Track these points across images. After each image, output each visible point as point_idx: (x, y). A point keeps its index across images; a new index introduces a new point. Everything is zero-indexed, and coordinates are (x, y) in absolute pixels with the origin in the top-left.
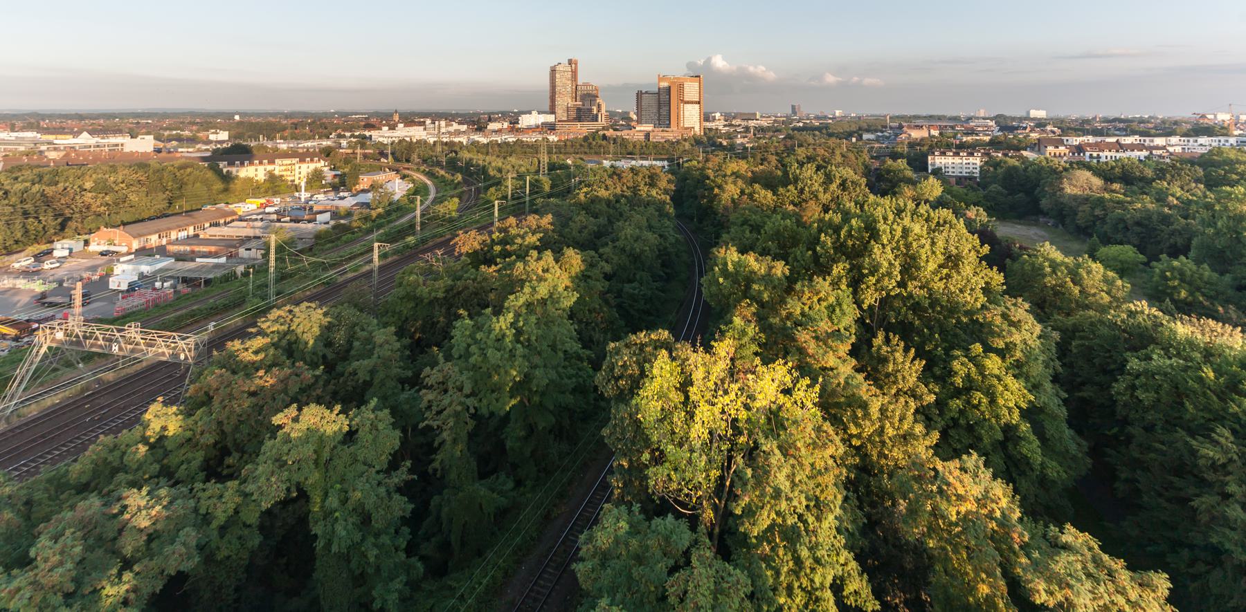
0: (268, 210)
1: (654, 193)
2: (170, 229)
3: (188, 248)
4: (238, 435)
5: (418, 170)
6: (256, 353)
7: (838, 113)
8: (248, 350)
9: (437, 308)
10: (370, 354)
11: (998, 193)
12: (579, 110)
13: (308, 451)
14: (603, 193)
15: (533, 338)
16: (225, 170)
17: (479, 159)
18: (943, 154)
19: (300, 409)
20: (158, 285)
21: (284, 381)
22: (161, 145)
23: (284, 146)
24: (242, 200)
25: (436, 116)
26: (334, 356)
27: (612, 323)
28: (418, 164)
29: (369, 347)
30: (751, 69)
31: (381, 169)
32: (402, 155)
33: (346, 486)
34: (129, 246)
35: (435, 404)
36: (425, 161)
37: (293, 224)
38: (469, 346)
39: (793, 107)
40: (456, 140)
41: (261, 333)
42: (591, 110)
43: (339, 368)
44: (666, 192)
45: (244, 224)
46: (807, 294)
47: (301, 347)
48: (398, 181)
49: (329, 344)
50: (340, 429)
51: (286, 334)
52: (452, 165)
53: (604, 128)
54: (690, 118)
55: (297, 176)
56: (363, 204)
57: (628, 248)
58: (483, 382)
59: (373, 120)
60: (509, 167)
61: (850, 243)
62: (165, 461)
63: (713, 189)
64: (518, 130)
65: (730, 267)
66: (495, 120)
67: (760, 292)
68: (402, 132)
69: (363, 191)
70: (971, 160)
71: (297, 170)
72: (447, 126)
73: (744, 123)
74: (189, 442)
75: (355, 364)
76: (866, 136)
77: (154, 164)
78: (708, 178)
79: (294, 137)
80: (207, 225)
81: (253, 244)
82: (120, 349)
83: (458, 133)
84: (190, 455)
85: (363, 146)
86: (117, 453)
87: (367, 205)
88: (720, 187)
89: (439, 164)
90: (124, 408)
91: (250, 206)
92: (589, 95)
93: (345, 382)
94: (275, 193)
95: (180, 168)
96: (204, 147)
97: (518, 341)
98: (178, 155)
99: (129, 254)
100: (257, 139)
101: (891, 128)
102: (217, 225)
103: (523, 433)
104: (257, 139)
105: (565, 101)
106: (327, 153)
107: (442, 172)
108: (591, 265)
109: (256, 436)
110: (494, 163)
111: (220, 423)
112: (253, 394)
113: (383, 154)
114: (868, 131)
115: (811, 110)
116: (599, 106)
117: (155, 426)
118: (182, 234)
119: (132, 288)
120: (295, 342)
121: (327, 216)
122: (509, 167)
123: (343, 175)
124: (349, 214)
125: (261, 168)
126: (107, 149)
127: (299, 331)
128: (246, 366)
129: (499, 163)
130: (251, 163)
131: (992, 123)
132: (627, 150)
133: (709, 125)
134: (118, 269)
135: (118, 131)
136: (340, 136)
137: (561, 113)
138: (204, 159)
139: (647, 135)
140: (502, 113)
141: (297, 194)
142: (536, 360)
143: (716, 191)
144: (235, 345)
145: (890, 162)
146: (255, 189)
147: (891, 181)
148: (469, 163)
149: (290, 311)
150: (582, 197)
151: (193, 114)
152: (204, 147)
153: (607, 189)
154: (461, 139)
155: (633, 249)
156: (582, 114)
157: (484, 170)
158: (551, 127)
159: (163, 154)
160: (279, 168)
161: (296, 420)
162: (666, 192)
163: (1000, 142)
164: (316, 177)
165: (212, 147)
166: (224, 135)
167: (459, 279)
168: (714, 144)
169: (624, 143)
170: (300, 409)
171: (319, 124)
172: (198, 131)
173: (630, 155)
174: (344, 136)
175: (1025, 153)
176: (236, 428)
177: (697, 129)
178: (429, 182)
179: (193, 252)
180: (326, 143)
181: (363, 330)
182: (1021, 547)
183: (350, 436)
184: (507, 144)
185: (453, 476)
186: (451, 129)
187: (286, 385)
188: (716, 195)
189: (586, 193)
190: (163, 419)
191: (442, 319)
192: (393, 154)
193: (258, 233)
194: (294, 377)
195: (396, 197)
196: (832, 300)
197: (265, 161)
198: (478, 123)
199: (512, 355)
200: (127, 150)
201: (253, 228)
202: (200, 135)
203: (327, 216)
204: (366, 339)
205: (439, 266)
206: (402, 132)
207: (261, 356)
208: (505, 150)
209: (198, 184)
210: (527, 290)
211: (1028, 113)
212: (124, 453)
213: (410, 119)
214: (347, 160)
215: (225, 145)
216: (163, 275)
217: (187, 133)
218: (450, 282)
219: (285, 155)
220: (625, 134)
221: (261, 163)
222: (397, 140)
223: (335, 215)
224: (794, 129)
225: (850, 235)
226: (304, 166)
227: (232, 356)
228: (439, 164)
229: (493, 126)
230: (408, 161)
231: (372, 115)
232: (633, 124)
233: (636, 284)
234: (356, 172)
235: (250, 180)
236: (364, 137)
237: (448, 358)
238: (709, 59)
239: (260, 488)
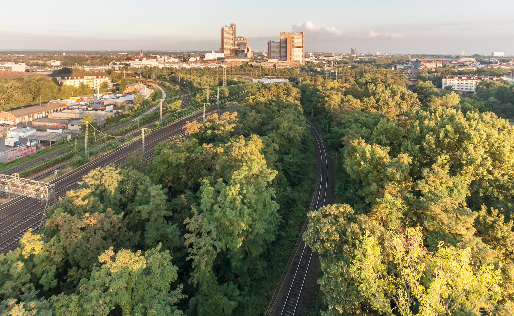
0: (81, 103)
1: (290, 99)
2: (34, 113)
3: (43, 124)
4: (75, 255)
5: (155, 83)
6: (83, 199)
7: (378, 53)
8: (79, 197)
9: (181, 169)
10: (148, 202)
11: (493, 102)
12: (237, 51)
13: (122, 283)
14: (263, 100)
15: (253, 201)
16: (60, 82)
17: (188, 77)
18: (452, 78)
19: (115, 252)
20: (28, 144)
21: (101, 222)
22: (29, 68)
23: (87, 69)
24: (68, 98)
25: (162, 54)
26: (126, 199)
27: (280, 180)
28: (155, 79)
29: (147, 195)
30: (328, 29)
31: (136, 82)
32: (146, 74)
33: (145, 305)
34: (15, 122)
35: (195, 244)
36: (158, 78)
37: (94, 112)
38: (213, 205)
39: (352, 50)
40: (174, 66)
41: (86, 186)
42: (243, 51)
43: (129, 207)
44: (296, 99)
45: (70, 111)
46: (432, 178)
47: (108, 194)
48: (146, 88)
49: (122, 192)
50: (142, 266)
51: (99, 186)
52: (173, 80)
53: (250, 61)
54: (297, 56)
55: (95, 85)
56: (129, 101)
57: (285, 134)
58: (225, 231)
59: (130, 56)
60: (205, 82)
61: (446, 141)
62: (34, 271)
63: (324, 98)
64: (205, 61)
65: (368, 155)
66: (192, 56)
67: (393, 174)
68: (146, 62)
69: (128, 94)
70: (469, 81)
71: (95, 82)
72: (168, 59)
73: (326, 59)
74: (48, 259)
75: (140, 208)
76: (398, 67)
77: (26, 78)
78: (318, 91)
79: (92, 64)
80: (52, 111)
81: (75, 122)
82: (9, 189)
83: (174, 63)
84: (48, 267)
85: (127, 69)
86: (6, 266)
87: (131, 102)
88: (328, 96)
89: (165, 79)
90: (12, 222)
91: (72, 101)
92: (242, 43)
93: (133, 217)
94: (84, 94)
95: (38, 81)
96: (50, 69)
97: (244, 204)
98: (37, 73)
99: (15, 126)
100: (74, 65)
101: (412, 62)
102: (56, 111)
103: (242, 257)
104: (74, 65)
105: (229, 46)
106: (109, 73)
107: (168, 84)
108: (267, 145)
109: (85, 256)
110: (196, 80)
111: (65, 248)
112: (83, 229)
113: (136, 74)
114: (399, 63)
115: (363, 51)
116: (248, 49)
117: (28, 249)
118: (40, 116)
119: (16, 145)
120: (104, 191)
121: (110, 108)
122: (205, 82)
123: (118, 85)
124: (122, 107)
125: (77, 81)
126: (4, 70)
127: (106, 185)
128: (78, 207)
129: (198, 80)
130: (72, 78)
131: (474, 60)
132: (265, 73)
133: (307, 59)
134: (9, 134)
135: (9, 60)
136: (114, 64)
137: (227, 53)
138: (50, 76)
139: (275, 65)
140: (195, 52)
141: (95, 95)
142: (256, 217)
143: (326, 99)
144: (71, 193)
145: (421, 82)
146: (74, 92)
147: (424, 94)
148: (182, 79)
149: (100, 171)
150: (251, 101)
151: (44, 52)
152: (50, 69)
153: (264, 97)
154: (176, 66)
155: (288, 134)
156: (238, 54)
157: (191, 83)
158: (222, 60)
159: (30, 73)
160: (86, 80)
161: (113, 259)
162: (296, 99)
163: (484, 71)
164: (104, 86)
165: (53, 69)
166: (58, 63)
167: (193, 151)
168: (312, 70)
169: (263, 69)
170: (115, 252)
171: (103, 58)
172: (46, 61)
173: (267, 76)
174: (116, 64)
175: (504, 78)
176: (74, 251)
177: (301, 62)
178: (162, 90)
179: (45, 126)
180: (108, 68)
181: (141, 184)
182: (117, 90)
183: (147, 271)
184: (200, 69)
185: (204, 288)
186: (171, 61)
187: (103, 224)
188: (326, 101)
189: (253, 99)
190: (32, 244)
191: (184, 176)
192: (142, 73)
193: (77, 116)
194: (106, 219)
195: (146, 98)
196: (451, 184)
197: (79, 77)
198: (184, 58)
199: (241, 214)
200: (13, 70)
201: (75, 113)
202: (47, 63)
203: (110, 108)
204: (144, 190)
205: (181, 144)
206: (146, 62)
207: (86, 201)
208: (201, 72)
209: (47, 89)
210: (245, 168)
211: (493, 53)
212: (10, 266)
213: (149, 55)
214: (119, 77)
215: (59, 68)
216: (31, 138)
217: (41, 62)
218: (188, 154)
219: (89, 74)
220: (262, 64)
221: (77, 78)
222: (143, 66)
223: (115, 107)
224: (355, 62)
225: (446, 136)
226: (98, 80)
227: (70, 201)
228: (165, 79)
229: (192, 59)
230: (149, 77)
231: (131, 53)
232: (265, 58)
233: (291, 156)
234: (124, 84)
235: (71, 87)
236: (127, 65)
237: (200, 212)
238: (305, 24)
239: (92, 307)
